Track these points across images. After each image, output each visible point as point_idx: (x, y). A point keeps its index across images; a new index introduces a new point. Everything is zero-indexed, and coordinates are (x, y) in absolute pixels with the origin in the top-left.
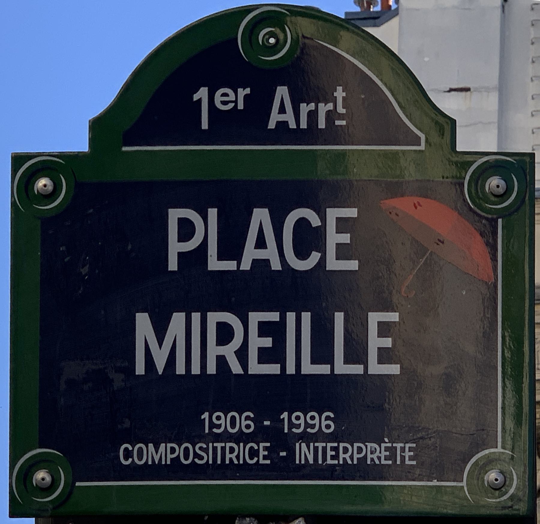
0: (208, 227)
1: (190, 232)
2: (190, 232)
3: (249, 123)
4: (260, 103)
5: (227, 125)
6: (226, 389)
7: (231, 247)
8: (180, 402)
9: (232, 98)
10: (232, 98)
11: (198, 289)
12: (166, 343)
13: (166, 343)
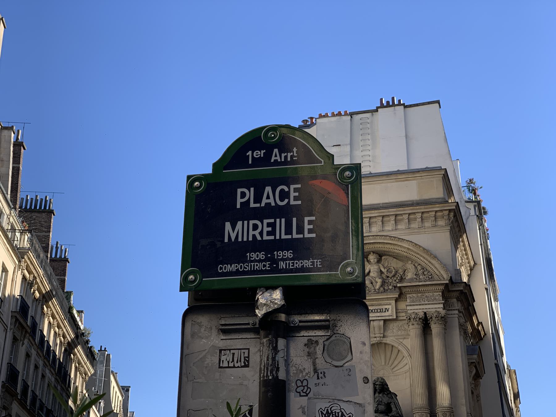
0: (250, 194)
1: (244, 196)
2: (244, 196)
3: (266, 160)
4: (269, 155)
5: (257, 162)
6: (256, 245)
7: (258, 199)
8: (239, 251)
9: (259, 154)
10: (259, 154)
11: (247, 213)
12: (234, 232)
13: (234, 232)
